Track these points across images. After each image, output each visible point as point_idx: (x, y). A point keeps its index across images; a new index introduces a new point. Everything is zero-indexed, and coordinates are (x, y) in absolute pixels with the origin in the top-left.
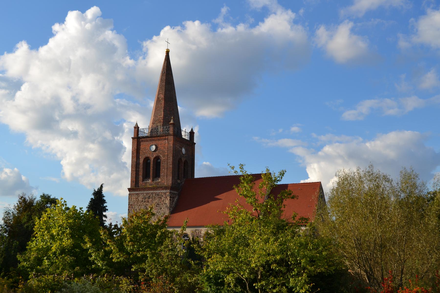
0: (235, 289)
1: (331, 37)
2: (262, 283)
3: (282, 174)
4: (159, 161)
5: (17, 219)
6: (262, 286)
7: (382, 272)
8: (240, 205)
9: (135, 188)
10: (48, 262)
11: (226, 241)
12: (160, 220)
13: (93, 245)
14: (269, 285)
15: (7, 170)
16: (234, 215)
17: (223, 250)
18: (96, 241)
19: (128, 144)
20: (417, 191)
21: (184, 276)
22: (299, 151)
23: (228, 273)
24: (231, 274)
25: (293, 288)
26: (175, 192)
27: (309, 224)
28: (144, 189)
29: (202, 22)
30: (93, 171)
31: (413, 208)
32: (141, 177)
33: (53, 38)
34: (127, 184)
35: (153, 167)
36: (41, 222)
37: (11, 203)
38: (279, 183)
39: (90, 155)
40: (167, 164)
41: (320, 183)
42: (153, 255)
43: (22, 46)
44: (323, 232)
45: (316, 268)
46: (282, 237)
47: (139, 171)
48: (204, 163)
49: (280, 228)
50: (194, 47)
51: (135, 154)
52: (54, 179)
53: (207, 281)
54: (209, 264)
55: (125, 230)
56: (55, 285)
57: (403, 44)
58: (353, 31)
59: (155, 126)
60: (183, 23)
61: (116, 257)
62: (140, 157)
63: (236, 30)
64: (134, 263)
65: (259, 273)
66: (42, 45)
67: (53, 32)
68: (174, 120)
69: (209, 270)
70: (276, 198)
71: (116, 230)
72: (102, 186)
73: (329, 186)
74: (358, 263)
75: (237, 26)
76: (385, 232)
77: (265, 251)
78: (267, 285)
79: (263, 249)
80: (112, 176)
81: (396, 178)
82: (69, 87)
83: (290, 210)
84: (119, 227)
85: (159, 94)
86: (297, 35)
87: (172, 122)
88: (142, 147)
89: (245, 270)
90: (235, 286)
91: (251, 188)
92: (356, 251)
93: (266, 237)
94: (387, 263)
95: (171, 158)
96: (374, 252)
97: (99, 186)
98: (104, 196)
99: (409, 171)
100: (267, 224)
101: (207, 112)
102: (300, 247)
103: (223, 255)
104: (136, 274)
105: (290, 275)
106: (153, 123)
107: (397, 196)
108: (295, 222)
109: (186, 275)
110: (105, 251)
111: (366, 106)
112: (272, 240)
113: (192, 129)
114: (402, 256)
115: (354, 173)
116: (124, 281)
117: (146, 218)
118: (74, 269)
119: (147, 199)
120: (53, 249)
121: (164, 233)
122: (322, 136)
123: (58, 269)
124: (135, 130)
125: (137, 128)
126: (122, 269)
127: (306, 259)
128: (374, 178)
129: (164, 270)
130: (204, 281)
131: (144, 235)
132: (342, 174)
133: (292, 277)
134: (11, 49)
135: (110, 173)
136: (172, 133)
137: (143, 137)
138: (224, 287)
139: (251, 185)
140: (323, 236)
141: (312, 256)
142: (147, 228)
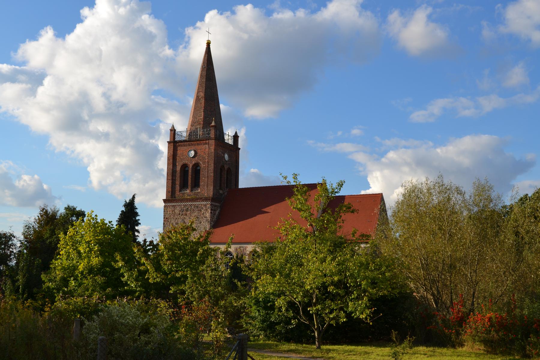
0: (287, 313)
1: (405, 25)
2: (317, 307)
3: (341, 185)
4: (198, 168)
5: (38, 234)
6: (318, 310)
7: (451, 296)
8: (293, 219)
9: (171, 199)
10: (75, 282)
11: (277, 259)
12: (201, 237)
13: (126, 263)
14: (325, 310)
15: (26, 177)
16: (287, 231)
17: (273, 270)
18: (129, 259)
19: (164, 147)
20: (492, 205)
21: (229, 299)
22: (360, 157)
23: (279, 296)
24: (283, 297)
25: (352, 313)
26: (217, 204)
27: (370, 242)
28: (182, 200)
29: (255, 6)
30: (124, 179)
31: (488, 224)
32: (178, 187)
33: (80, 24)
34: (163, 195)
35: (191, 176)
36: (67, 238)
37: (31, 216)
38: (337, 195)
39: (123, 161)
40: (208, 172)
41: (381, 195)
42: (194, 275)
43: (47, 32)
44: (385, 250)
45: (378, 290)
46: (340, 256)
47: (175, 180)
48: (252, 170)
49: (338, 245)
50: (246, 36)
51: (171, 161)
52: (79, 188)
53: (255, 304)
54: (258, 285)
55: (163, 247)
56: (85, 308)
57: (487, 33)
58: (429, 17)
59: (193, 128)
60: (233, 8)
61: (153, 277)
62: (177, 164)
63: (295, 16)
64: (171, 285)
65: (314, 296)
66: (69, 33)
67: (81, 17)
68: (215, 122)
69: (257, 292)
70: (333, 212)
71: (151, 247)
72: (134, 197)
73: (393, 197)
74: (425, 285)
75: (295, 11)
76: (456, 251)
77: (322, 271)
78: (323, 309)
79: (319, 270)
80: (147, 185)
81: (469, 190)
82: (99, 82)
83: (348, 225)
84: (155, 243)
85: (198, 92)
86: (367, 22)
87: (213, 124)
88: (179, 152)
89: (298, 293)
90: (287, 310)
91: (306, 200)
92: (422, 272)
93: (322, 256)
94: (456, 286)
95: (213, 165)
96: (442, 274)
97: (131, 197)
98: (136, 208)
99: (483, 182)
100: (323, 241)
101: (257, 112)
102: (360, 267)
103: (274, 276)
104: (174, 297)
105: (349, 298)
106: (192, 126)
107: (469, 210)
108: (354, 239)
109: (231, 298)
110: (139, 271)
111: (437, 107)
112: (329, 259)
113: (236, 133)
114: (474, 278)
115: (422, 184)
116: (162, 305)
117: (186, 234)
118: (105, 290)
119: (184, 212)
120: (81, 268)
121: (206, 251)
122: (387, 141)
123: (88, 291)
124: (171, 133)
125: (173, 131)
126: (160, 291)
127: (367, 281)
128: (444, 190)
129: (207, 292)
130: (252, 304)
131: (184, 253)
132: (409, 186)
133: (351, 300)
134: (34, 36)
135: (145, 181)
136: (213, 136)
137: (181, 141)
138: (274, 311)
139: (305, 197)
140: (386, 254)
141: (374, 277)
142: (187, 245)
